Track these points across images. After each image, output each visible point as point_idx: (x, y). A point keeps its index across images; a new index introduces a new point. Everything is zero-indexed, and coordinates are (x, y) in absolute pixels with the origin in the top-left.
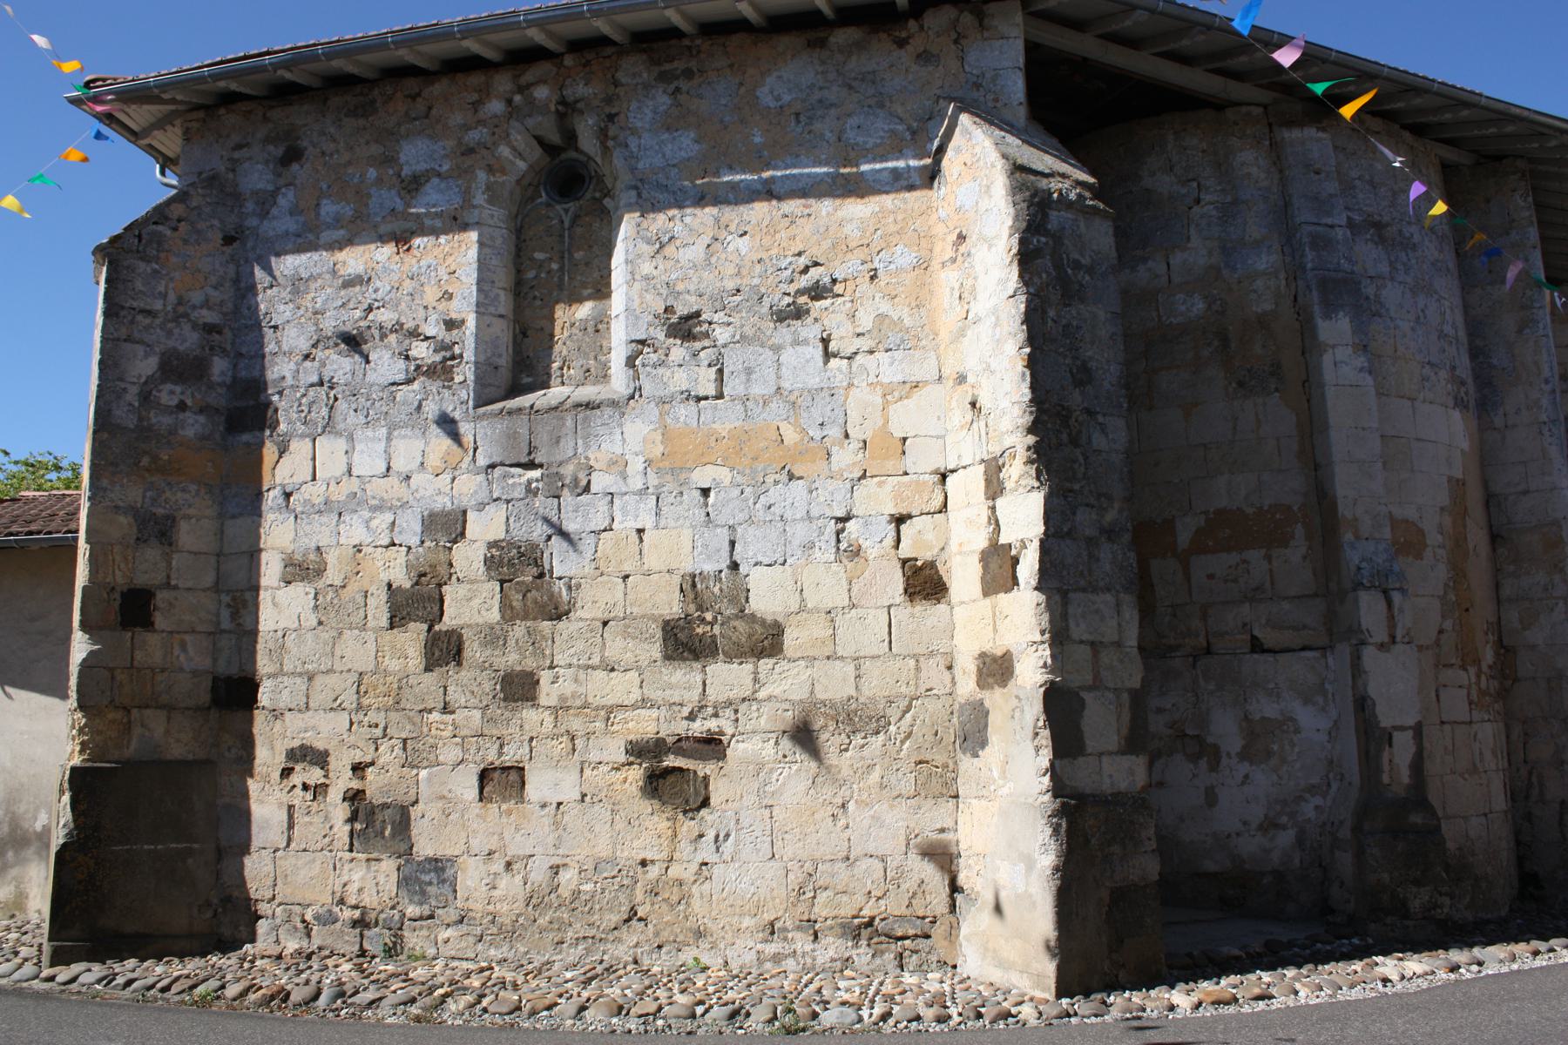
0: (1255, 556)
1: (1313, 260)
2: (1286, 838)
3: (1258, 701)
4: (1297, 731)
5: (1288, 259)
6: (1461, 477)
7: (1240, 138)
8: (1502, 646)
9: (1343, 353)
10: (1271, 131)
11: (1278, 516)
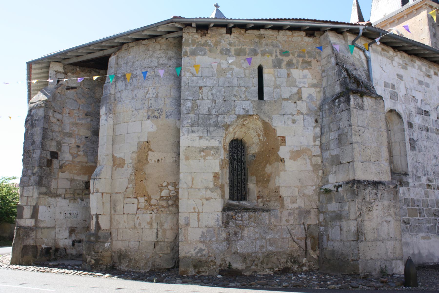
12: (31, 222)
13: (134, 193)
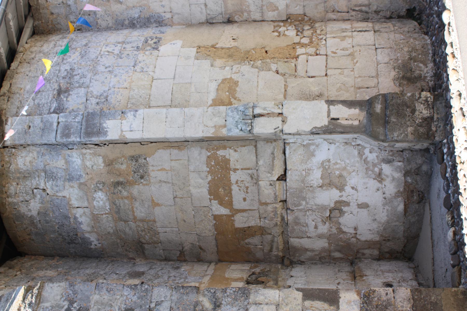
0: (234, 177)
1: (76, 137)
2: (387, 169)
3: (312, 180)
4: (329, 161)
5: (75, 147)
6: (195, 50)
7: (11, 164)
8: (287, 20)
9: (126, 125)
10: (7, 147)
11: (213, 163)
12: (349, 302)
13: (288, 60)
